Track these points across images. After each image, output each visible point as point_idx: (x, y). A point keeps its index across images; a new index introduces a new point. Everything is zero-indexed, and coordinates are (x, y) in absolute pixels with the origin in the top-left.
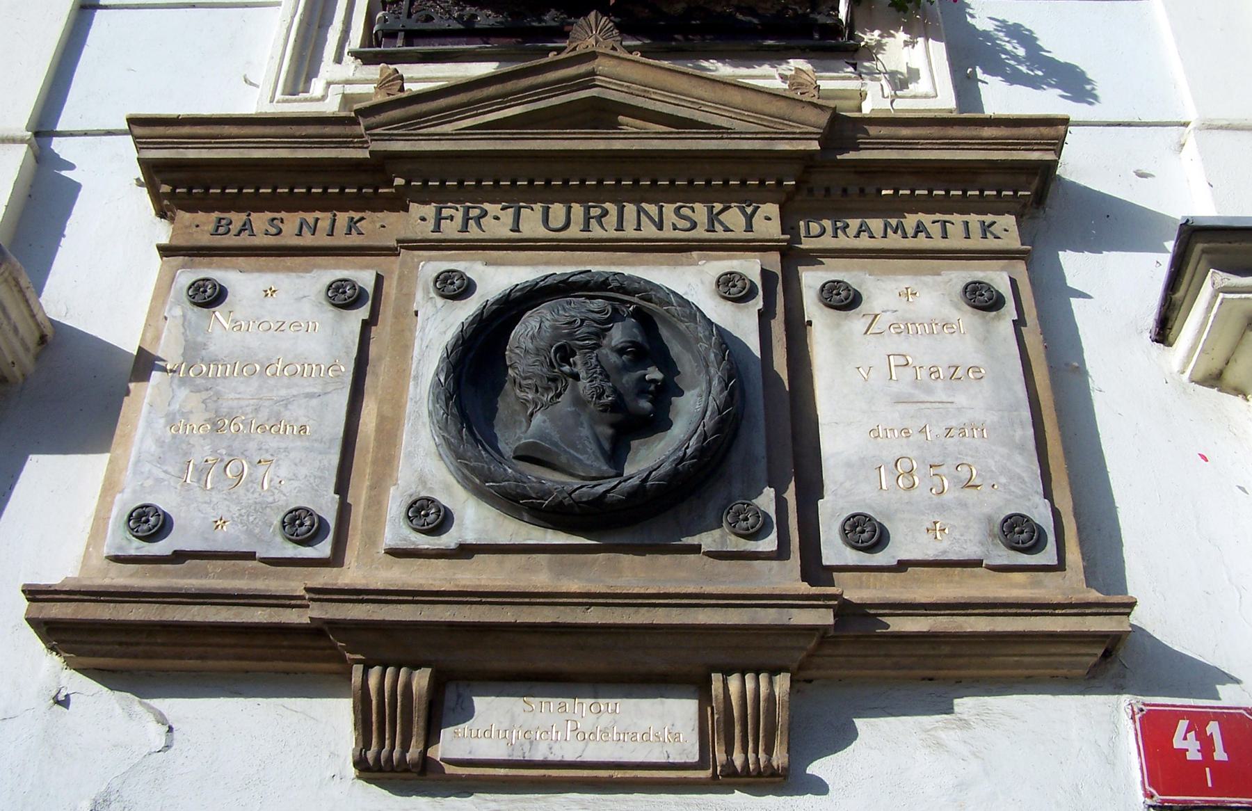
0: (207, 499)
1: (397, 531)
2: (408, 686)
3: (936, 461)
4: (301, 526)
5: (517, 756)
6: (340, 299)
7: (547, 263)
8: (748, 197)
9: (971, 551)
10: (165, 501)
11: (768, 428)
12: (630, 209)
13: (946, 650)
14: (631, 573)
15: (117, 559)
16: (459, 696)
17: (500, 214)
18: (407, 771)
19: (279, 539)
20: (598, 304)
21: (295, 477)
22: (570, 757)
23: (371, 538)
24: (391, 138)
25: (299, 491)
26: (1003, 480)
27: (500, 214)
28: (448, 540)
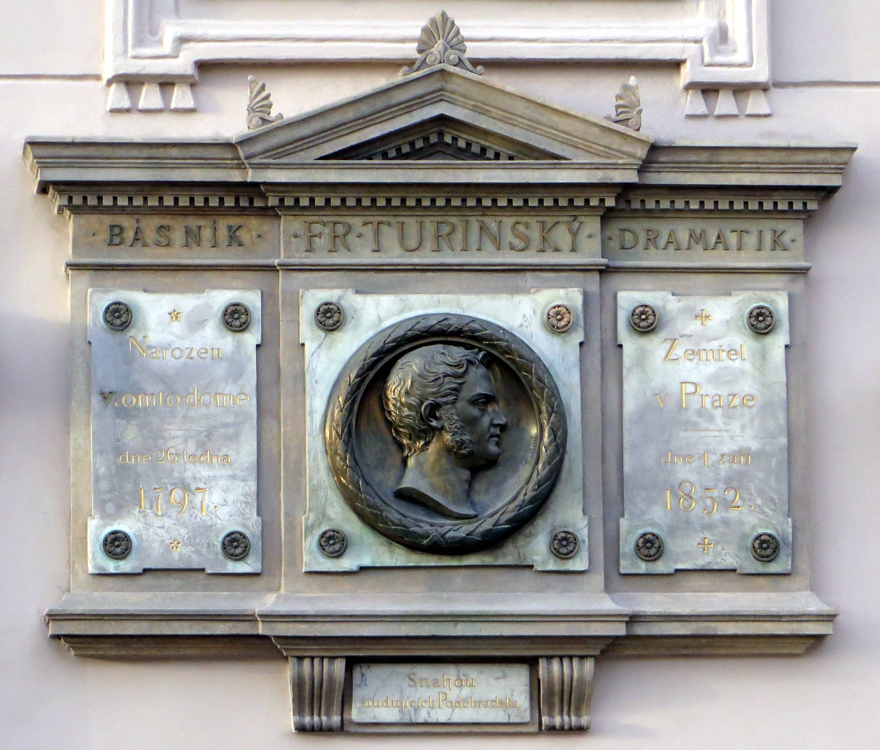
0: (160, 524)
1: (313, 558)
3: (710, 484)
9: (729, 561)
11: (617, 199)
16: (363, 675)
21: (225, 503)
22: (442, 719)
23: (294, 559)
25: (231, 516)
26: (759, 502)
28: (347, 563)
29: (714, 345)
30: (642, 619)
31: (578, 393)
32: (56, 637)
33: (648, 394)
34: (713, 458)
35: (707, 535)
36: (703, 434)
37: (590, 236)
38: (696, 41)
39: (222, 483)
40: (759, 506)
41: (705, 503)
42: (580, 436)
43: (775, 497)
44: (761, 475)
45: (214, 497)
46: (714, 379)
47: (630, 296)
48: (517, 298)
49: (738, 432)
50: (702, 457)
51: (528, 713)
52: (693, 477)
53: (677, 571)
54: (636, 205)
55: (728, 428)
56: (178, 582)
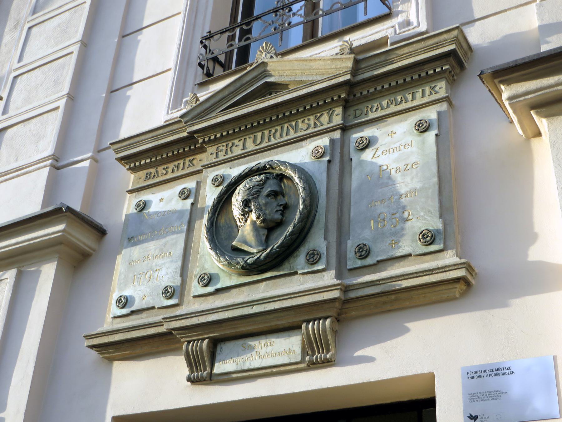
2: (201, 348)
3: (394, 212)
4: (169, 293)
5: (239, 369)
6: (421, 129)
7: (247, 163)
8: (327, 106)
10: (127, 293)
12: (266, 132)
13: (393, 297)
14: (264, 290)
15: (115, 317)
16: (221, 348)
17: (239, 143)
18: (205, 380)
19: (162, 298)
20: (263, 177)
22: (257, 366)
24: (193, 125)
26: (422, 214)
27: (239, 143)
29: (397, 145)
30: (351, 288)
31: (325, 183)
32: (92, 347)
33: (364, 176)
34: (396, 197)
35: (393, 238)
36: (390, 187)
37: (337, 115)
38: (393, 27)
39: (167, 265)
40: (423, 216)
41: (392, 221)
42: (325, 202)
43: (431, 209)
44: (423, 200)
45: (163, 272)
46: (397, 160)
47: (356, 136)
48: (300, 150)
49: (409, 181)
50: (390, 199)
51: (300, 356)
52: (385, 210)
53: (379, 262)
54: (358, 95)
55: (404, 181)
56: (145, 315)
